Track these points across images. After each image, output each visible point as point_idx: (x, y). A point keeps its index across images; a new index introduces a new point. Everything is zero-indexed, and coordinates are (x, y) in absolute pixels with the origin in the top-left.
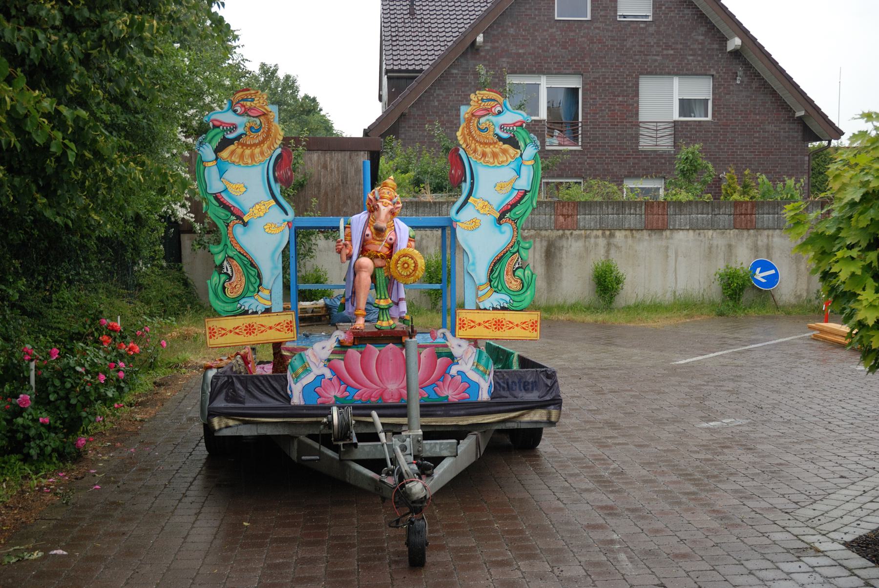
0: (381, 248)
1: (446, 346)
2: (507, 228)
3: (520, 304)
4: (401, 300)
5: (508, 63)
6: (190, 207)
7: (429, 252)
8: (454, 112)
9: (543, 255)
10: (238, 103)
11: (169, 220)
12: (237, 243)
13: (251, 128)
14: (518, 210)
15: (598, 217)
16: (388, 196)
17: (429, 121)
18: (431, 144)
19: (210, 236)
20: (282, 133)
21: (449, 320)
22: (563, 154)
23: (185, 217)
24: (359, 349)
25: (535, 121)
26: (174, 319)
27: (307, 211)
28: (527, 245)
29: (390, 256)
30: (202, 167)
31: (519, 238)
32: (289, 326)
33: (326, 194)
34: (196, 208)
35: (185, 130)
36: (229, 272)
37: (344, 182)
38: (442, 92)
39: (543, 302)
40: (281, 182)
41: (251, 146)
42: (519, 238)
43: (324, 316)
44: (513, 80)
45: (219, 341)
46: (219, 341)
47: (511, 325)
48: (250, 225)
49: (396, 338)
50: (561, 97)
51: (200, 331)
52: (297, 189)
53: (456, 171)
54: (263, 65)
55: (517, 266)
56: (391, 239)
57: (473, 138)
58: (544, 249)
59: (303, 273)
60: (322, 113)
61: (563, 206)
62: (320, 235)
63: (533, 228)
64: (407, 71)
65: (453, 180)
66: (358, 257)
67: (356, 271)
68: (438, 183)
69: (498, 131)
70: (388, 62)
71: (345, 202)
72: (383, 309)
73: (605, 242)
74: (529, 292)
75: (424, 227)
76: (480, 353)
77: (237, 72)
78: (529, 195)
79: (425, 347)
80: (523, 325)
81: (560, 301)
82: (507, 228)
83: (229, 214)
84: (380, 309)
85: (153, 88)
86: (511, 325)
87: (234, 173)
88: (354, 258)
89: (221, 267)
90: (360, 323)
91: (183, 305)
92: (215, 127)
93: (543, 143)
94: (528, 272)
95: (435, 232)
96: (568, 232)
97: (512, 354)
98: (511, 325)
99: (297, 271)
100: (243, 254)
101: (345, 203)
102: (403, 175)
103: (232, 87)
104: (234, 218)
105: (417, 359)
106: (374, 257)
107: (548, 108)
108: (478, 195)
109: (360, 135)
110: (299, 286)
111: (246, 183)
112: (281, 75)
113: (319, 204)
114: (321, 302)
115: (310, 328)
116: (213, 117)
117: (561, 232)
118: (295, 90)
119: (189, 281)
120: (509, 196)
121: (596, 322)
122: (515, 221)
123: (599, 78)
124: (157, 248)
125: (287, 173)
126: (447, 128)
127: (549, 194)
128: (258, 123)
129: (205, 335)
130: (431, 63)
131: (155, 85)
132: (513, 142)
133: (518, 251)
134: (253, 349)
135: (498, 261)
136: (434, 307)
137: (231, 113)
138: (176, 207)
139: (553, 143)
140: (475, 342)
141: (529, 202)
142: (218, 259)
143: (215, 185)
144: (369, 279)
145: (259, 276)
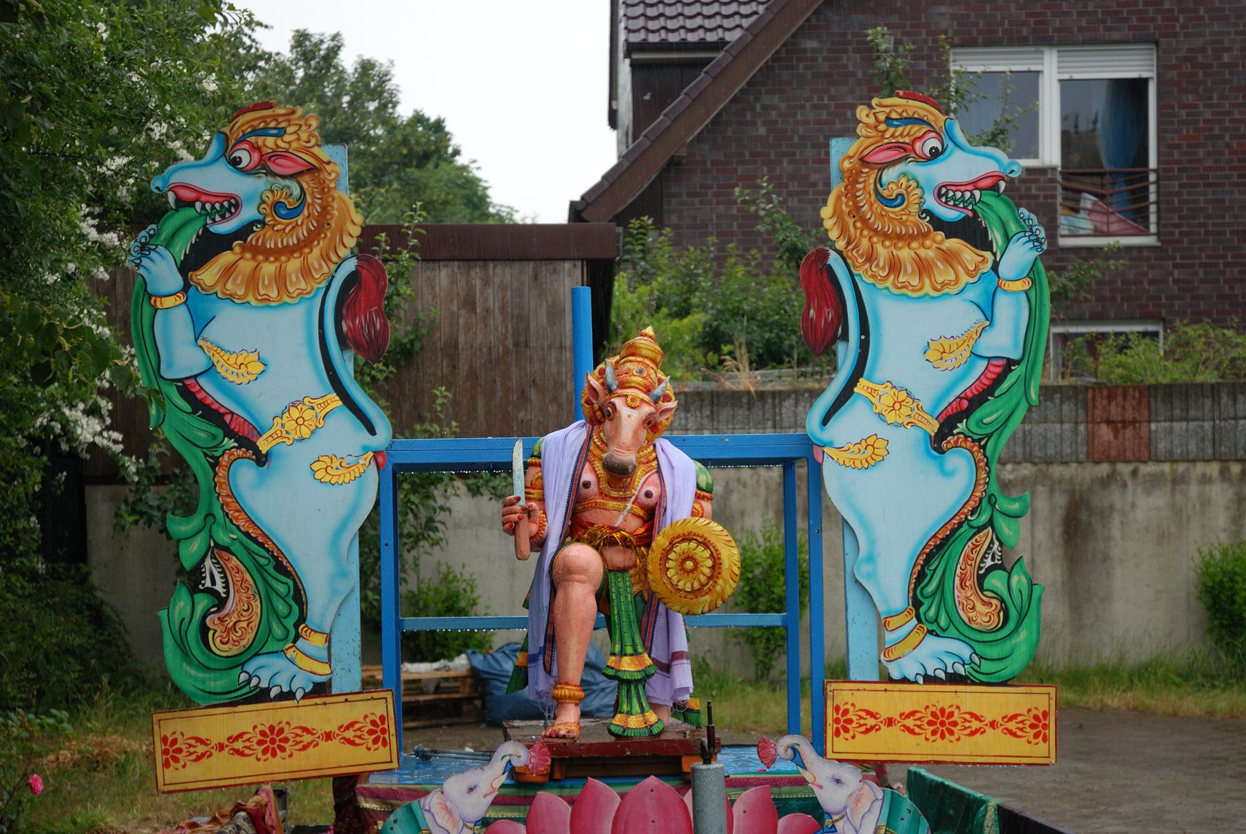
0: (625, 519)
1: (802, 782)
2: (960, 462)
3: (1000, 665)
4: (677, 656)
5: (953, 17)
6: (111, 414)
7: (748, 523)
8: (810, 152)
9: (1058, 531)
10: (242, 140)
11: (56, 450)
12: (241, 510)
13: (276, 206)
14: (990, 413)
15: (1207, 425)
16: (641, 379)
17: (740, 178)
18: (749, 240)
19: (163, 489)
20: (358, 218)
21: (805, 705)
22: (1107, 258)
23: (98, 440)
24: (567, 792)
25: (1029, 170)
26: (64, 714)
27: (421, 420)
28: (1015, 507)
29: (646, 540)
30: (147, 310)
31: (994, 488)
32: (377, 730)
33: (472, 374)
34: (130, 417)
35: (97, 210)
36: (219, 587)
37: (521, 343)
38: (776, 100)
39: (1060, 659)
40: (359, 348)
41: (277, 253)
42: (994, 488)
43: (469, 700)
44: (968, 63)
45: (189, 773)
46: (189, 773)
47: (975, 724)
48: (274, 462)
49: (666, 760)
50: (1099, 105)
51: (136, 745)
52: (397, 364)
53: (819, 311)
54: (301, 38)
55: (989, 562)
56: (648, 495)
57: (865, 222)
58: (1059, 515)
59: (412, 585)
60: (460, 160)
61: (1111, 398)
62: (458, 483)
63: (1029, 459)
64: (683, 46)
65: (811, 334)
66: (562, 544)
67: (556, 579)
68: (768, 343)
69: (931, 203)
70: (633, 25)
71: (521, 396)
72: (628, 682)
73: (1230, 493)
74: (1023, 634)
75: (736, 463)
76: (894, 802)
77: (234, 55)
78: (1018, 371)
79: (743, 784)
80: (1010, 725)
81: (1108, 655)
82: (960, 462)
83: (219, 433)
84: (622, 682)
85: (16, 103)
86: (977, 725)
87: (234, 327)
88: (552, 545)
89: (198, 570)
90: (569, 720)
91: (89, 676)
92: (182, 203)
93: (1052, 228)
94: (1018, 580)
95: (762, 471)
96: (1125, 469)
97: (982, 802)
98: (977, 725)
99: (397, 582)
100: (258, 539)
101: (524, 396)
102: (676, 323)
103: (224, 97)
104: (232, 443)
105: (723, 818)
106: (603, 543)
107: (1065, 135)
108: (880, 375)
109: (560, 216)
110: (404, 618)
111: (263, 350)
112: (348, 61)
113: (456, 403)
114: (461, 663)
115: (431, 733)
116: (177, 178)
117: (1105, 468)
118: (387, 101)
119: (108, 610)
120: (962, 377)
121: (1211, 713)
122: (980, 443)
123: (1202, 50)
124: (21, 524)
125: (371, 324)
126: (790, 194)
127: (1068, 366)
128: (296, 191)
129: (151, 755)
130: (746, 23)
131: (22, 93)
132: (972, 232)
133: (990, 523)
134: (280, 794)
135: (936, 550)
136: (762, 675)
137: (222, 169)
138: (75, 414)
139: (1080, 230)
140: (877, 770)
141: (1019, 390)
142: (190, 552)
143: (182, 359)
144: (592, 601)
145: (299, 596)
